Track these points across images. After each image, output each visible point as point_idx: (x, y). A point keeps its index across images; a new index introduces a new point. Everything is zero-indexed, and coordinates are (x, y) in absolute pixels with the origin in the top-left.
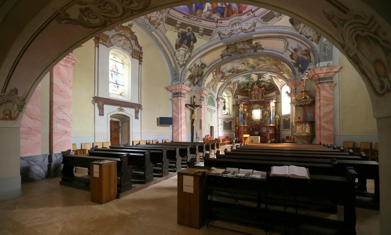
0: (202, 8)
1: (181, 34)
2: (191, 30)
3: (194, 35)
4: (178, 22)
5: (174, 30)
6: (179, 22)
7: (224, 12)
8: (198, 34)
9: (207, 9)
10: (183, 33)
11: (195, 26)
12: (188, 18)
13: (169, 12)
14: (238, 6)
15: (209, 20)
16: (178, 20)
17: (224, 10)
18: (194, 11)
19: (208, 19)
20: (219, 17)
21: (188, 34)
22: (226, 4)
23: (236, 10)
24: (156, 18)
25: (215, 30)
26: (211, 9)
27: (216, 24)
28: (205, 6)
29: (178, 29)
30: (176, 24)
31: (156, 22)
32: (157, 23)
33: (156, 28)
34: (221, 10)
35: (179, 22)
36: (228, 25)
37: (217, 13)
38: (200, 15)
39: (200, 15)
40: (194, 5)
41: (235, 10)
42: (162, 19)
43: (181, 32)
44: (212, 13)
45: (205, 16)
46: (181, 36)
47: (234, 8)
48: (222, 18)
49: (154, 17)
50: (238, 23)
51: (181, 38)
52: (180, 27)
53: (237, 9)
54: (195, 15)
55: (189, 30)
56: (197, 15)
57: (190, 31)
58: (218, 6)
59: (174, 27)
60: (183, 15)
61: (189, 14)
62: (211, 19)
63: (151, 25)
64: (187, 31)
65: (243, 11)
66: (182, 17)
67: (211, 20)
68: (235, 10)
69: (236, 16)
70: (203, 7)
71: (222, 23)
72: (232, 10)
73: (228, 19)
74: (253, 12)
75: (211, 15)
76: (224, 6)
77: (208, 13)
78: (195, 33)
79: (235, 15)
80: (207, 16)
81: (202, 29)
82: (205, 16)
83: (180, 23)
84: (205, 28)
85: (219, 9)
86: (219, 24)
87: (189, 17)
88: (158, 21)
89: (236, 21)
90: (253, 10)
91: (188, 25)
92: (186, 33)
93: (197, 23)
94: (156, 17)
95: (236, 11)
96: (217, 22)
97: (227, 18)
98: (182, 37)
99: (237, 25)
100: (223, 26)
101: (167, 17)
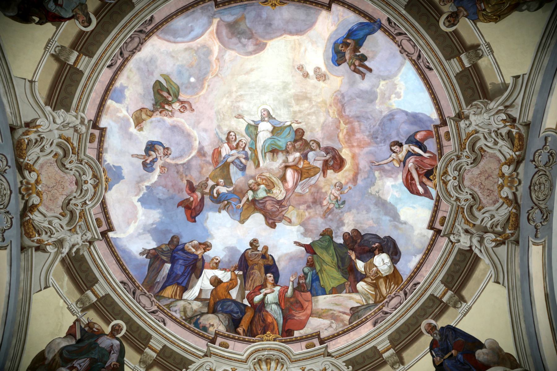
0: (184, 284)
1: (82, 330)
2: (123, 332)
3: (122, 353)
4: (97, 287)
5: (72, 301)
6: (101, 289)
7: (241, 319)
8: (138, 357)
9: (197, 294)
10: (91, 328)
11: (139, 327)
12: (134, 293)
13: (91, 243)
14: (282, 312)
15: (192, 326)
16: (101, 280)
17: (243, 313)
18: (158, 283)
19: (190, 323)
20: (222, 329)
21: (105, 342)
22: (253, 299)
23: (275, 323)
24: (46, 224)
25: (198, 362)
26: (209, 297)
27: (207, 345)
28: (196, 283)
29: (84, 310)
30: (90, 288)
31: (39, 235)
32: (39, 241)
33: (23, 249)
34: (236, 310)
35: (101, 289)
36: (244, 357)
37: (219, 315)
38: (171, 300)
39: (171, 300)
40: (168, 266)
41: (272, 323)
42: (60, 243)
43: (88, 325)
44: (205, 310)
45: (185, 311)
46: (78, 336)
47: (270, 315)
48: (232, 335)
49: (45, 216)
50: (278, 362)
51: (74, 342)
52: (93, 306)
53: (281, 321)
54: (158, 296)
55: (116, 330)
56: (164, 297)
57: (119, 336)
58: (228, 297)
59: (78, 296)
60: (124, 279)
61: (142, 285)
62: (196, 324)
63: (16, 222)
64: (107, 330)
65: (295, 332)
66: (118, 282)
67: (197, 330)
68: (272, 323)
69: (275, 340)
70: (188, 284)
71: (227, 347)
72: (264, 320)
73: (249, 342)
74: (322, 342)
75: (202, 314)
76: (246, 302)
77: (196, 305)
78: (129, 351)
79: (272, 336)
80: (189, 314)
81: (159, 347)
82: (185, 311)
83: (102, 293)
84: (169, 345)
85: (229, 306)
86: (216, 349)
87: (138, 292)
88: (44, 237)
89: (271, 353)
90: (322, 336)
91: (121, 315)
92: (101, 334)
93: (151, 320)
94: (50, 223)
95: (276, 325)
96: (213, 341)
97: (247, 338)
98: (78, 342)
99: (273, 364)
100: (229, 358)
101: (78, 250)
